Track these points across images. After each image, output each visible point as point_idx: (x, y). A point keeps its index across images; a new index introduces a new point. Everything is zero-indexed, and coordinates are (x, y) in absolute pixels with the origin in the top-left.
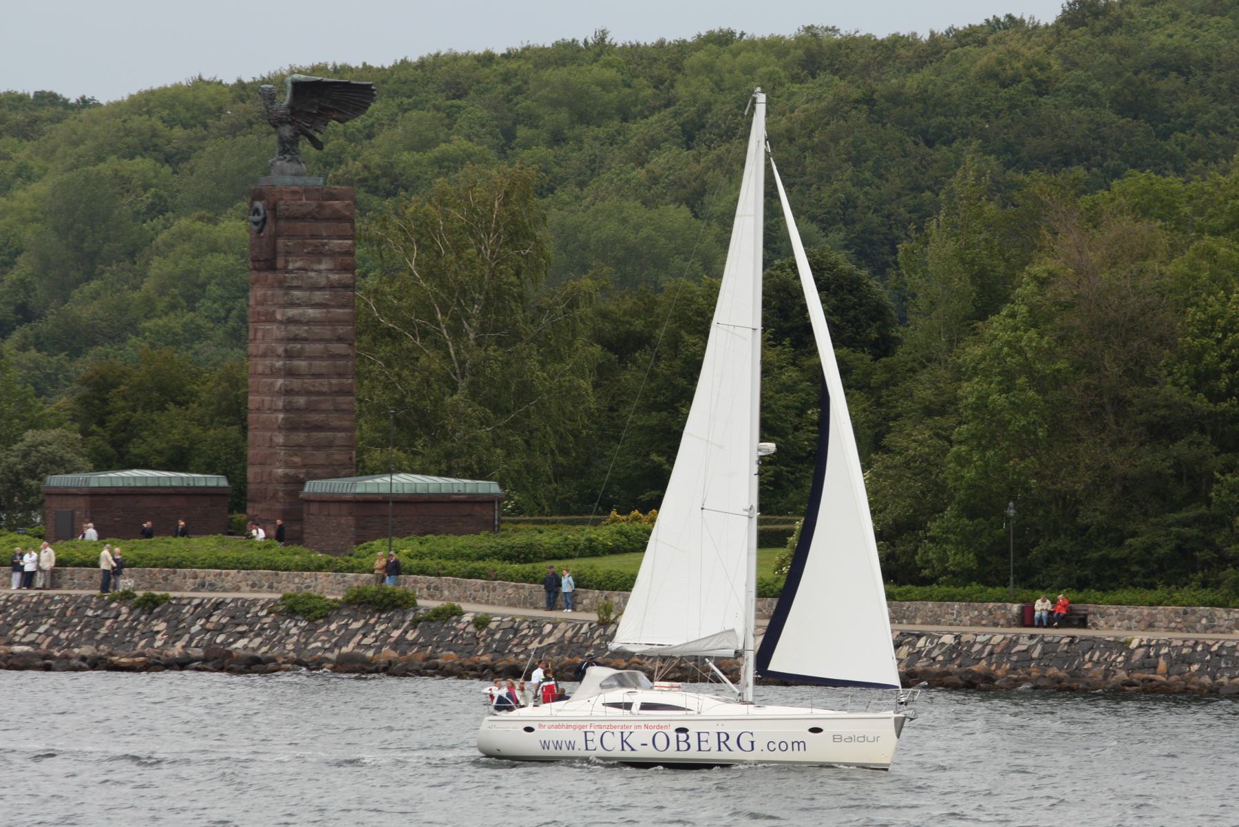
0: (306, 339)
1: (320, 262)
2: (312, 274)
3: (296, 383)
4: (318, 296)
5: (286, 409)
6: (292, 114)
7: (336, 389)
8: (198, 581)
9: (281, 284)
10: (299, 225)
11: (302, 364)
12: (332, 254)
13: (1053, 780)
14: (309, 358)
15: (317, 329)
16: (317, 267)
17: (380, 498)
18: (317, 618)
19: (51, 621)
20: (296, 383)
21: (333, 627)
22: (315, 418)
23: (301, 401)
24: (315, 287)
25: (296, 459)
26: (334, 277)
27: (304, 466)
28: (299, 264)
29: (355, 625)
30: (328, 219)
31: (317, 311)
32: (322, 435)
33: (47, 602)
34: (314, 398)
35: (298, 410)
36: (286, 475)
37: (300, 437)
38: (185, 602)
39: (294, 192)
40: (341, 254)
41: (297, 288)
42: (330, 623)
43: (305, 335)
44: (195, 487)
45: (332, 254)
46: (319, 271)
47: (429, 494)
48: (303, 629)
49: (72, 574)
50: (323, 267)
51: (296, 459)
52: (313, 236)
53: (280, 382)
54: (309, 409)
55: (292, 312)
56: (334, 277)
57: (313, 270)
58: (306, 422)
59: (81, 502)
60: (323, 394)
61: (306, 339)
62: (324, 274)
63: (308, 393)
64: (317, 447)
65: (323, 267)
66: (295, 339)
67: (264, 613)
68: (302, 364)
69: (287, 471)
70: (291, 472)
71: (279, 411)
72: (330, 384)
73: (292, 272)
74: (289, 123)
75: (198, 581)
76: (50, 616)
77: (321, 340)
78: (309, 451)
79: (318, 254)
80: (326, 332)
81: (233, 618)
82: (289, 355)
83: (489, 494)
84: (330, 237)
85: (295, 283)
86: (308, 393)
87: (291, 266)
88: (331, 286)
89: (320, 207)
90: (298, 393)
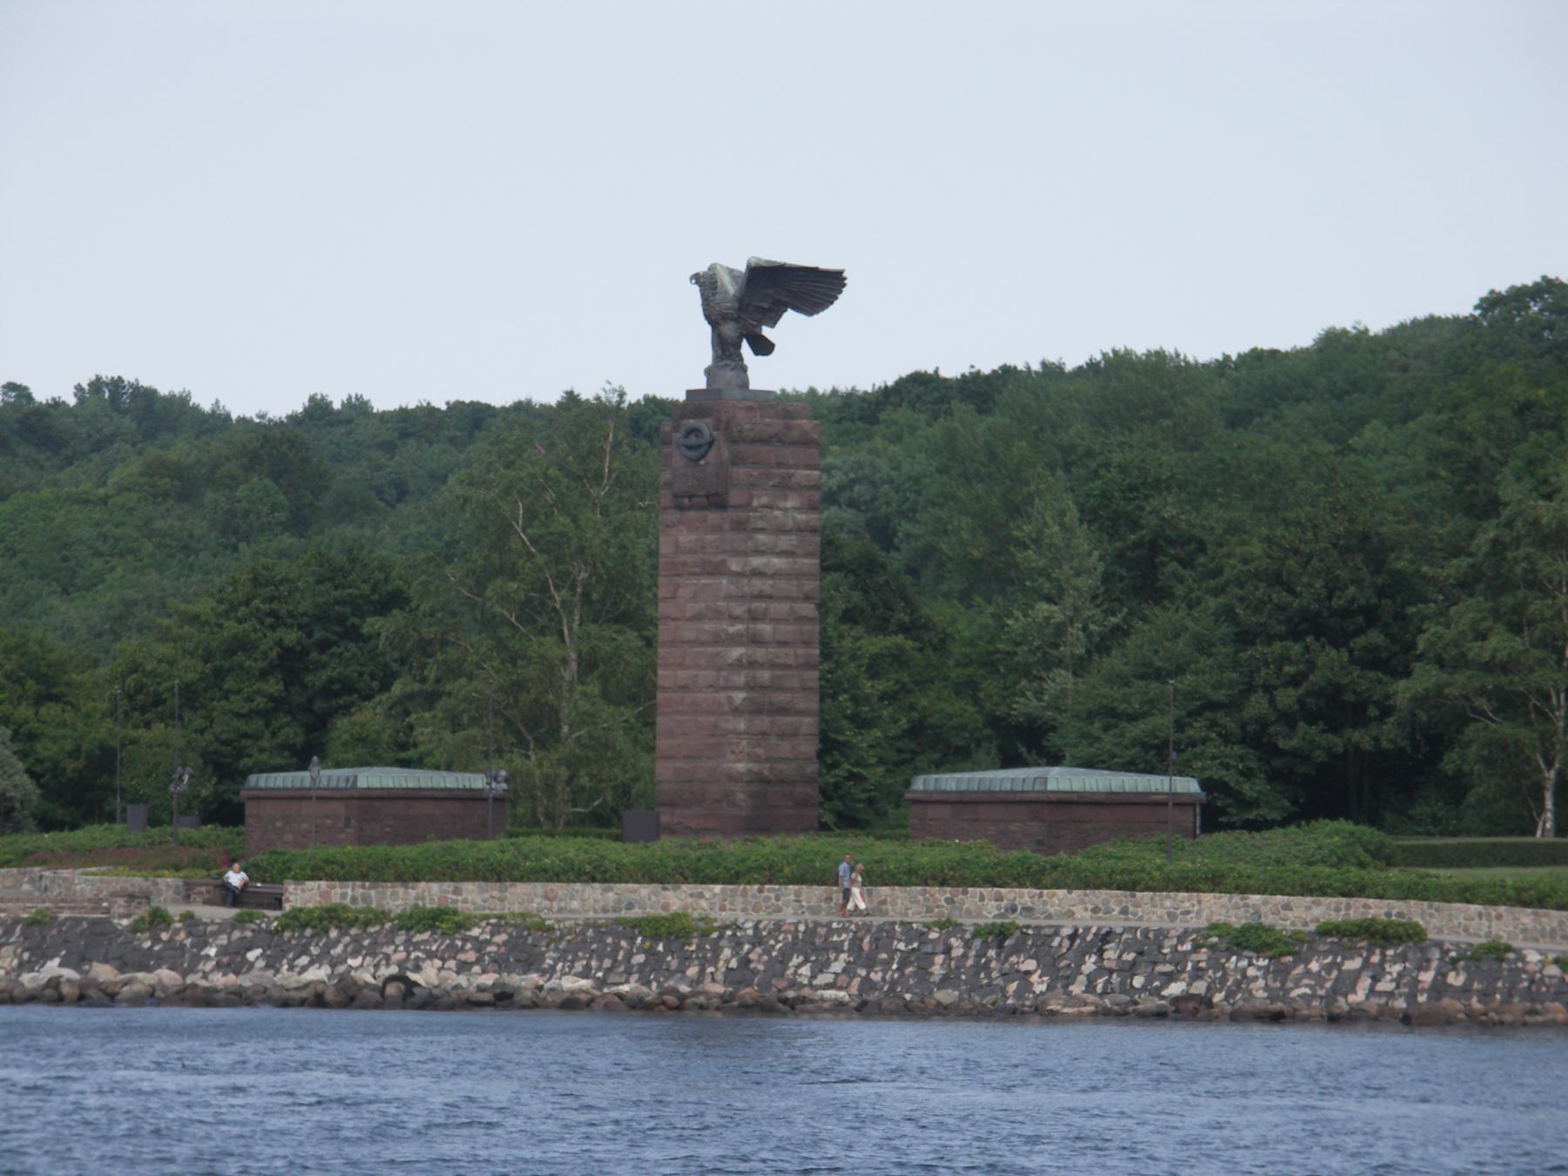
0: (770, 597)
1: (785, 498)
2: (778, 513)
3: (760, 654)
4: (785, 542)
5: (749, 686)
6: (740, 309)
7: (801, 660)
8: (1004, 904)
9: (739, 526)
10: (765, 449)
11: (766, 628)
12: (800, 488)
13: (107, 1149)
14: (775, 621)
15: (782, 584)
16: (781, 504)
17: (1075, 798)
18: (1281, 955)
19: (843, 956)
20: (760, 654)
21: (1314, 966)
22: (781, 698)
23: (765, 676)
24: (781, 530)
25: (760, 751)
26: (801, 517)
27: (768, 760)
28: (765, 500)
29: (1353, 964)
30: (794, 443)
31: (784, 560)
32: (787, 719)
33: (822, 931)
34: (778, 673)
35: (762, 687)
36: (749, 771)
37: (763, 722)
38: (1049, 931)
39: (750, 409)
40: (808, 488)
41: (762, 530)
42: (1307, 962)
43: (770, 591)
44: (471, 790)
45: (800, 488)
46: (785, 510)
47: (1125, 793)
48: (1266, 970)
49: (798, 894)
50: (789, 504)
51: (760, 751)
52: (780, 465)
53: (736, 652)
54: (775, 686)
55: (757, 562)
56: (801, 517)
57: (779, 508)
58: (771, 704)
59: (340, 808)
60: (786, 667)
61: (770, 597)
62: (790, 514)
63: (773, 665)
64: (783, 736)
65: (789, 504)
66: (760, 596)
67: (1187, 946)
68: (766, 628)
69: (750, 766)
70: (754, 767)
71: (739, 689)
72: (796, 655)
73: (755, 510)
74: (736, 320)
75: (1004, 904)
76: (838, 949)
77: (787, 598)
78: (773, 740)
79: (784, 486)
80: (790, 587)
81: (1140, 953)
82: (754, 617)
83: (1189, 794)
84: (796, 466)
85: (760, 524)
86: (773, 665)
87: (755, 503)
88: (799, 530)
89: (788, 427)
90: (762, 666)
